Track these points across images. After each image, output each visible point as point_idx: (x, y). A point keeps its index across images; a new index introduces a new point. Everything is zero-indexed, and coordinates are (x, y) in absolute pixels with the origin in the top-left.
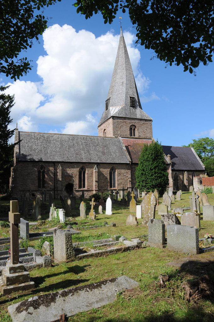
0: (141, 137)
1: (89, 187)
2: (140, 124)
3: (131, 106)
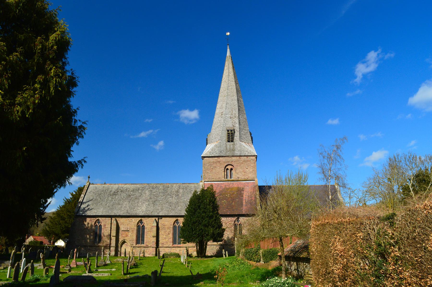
0: (240, 179)
1: (147, 244)
2: (238, 162)
3: (229, 141)
